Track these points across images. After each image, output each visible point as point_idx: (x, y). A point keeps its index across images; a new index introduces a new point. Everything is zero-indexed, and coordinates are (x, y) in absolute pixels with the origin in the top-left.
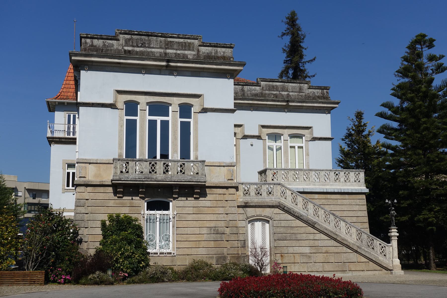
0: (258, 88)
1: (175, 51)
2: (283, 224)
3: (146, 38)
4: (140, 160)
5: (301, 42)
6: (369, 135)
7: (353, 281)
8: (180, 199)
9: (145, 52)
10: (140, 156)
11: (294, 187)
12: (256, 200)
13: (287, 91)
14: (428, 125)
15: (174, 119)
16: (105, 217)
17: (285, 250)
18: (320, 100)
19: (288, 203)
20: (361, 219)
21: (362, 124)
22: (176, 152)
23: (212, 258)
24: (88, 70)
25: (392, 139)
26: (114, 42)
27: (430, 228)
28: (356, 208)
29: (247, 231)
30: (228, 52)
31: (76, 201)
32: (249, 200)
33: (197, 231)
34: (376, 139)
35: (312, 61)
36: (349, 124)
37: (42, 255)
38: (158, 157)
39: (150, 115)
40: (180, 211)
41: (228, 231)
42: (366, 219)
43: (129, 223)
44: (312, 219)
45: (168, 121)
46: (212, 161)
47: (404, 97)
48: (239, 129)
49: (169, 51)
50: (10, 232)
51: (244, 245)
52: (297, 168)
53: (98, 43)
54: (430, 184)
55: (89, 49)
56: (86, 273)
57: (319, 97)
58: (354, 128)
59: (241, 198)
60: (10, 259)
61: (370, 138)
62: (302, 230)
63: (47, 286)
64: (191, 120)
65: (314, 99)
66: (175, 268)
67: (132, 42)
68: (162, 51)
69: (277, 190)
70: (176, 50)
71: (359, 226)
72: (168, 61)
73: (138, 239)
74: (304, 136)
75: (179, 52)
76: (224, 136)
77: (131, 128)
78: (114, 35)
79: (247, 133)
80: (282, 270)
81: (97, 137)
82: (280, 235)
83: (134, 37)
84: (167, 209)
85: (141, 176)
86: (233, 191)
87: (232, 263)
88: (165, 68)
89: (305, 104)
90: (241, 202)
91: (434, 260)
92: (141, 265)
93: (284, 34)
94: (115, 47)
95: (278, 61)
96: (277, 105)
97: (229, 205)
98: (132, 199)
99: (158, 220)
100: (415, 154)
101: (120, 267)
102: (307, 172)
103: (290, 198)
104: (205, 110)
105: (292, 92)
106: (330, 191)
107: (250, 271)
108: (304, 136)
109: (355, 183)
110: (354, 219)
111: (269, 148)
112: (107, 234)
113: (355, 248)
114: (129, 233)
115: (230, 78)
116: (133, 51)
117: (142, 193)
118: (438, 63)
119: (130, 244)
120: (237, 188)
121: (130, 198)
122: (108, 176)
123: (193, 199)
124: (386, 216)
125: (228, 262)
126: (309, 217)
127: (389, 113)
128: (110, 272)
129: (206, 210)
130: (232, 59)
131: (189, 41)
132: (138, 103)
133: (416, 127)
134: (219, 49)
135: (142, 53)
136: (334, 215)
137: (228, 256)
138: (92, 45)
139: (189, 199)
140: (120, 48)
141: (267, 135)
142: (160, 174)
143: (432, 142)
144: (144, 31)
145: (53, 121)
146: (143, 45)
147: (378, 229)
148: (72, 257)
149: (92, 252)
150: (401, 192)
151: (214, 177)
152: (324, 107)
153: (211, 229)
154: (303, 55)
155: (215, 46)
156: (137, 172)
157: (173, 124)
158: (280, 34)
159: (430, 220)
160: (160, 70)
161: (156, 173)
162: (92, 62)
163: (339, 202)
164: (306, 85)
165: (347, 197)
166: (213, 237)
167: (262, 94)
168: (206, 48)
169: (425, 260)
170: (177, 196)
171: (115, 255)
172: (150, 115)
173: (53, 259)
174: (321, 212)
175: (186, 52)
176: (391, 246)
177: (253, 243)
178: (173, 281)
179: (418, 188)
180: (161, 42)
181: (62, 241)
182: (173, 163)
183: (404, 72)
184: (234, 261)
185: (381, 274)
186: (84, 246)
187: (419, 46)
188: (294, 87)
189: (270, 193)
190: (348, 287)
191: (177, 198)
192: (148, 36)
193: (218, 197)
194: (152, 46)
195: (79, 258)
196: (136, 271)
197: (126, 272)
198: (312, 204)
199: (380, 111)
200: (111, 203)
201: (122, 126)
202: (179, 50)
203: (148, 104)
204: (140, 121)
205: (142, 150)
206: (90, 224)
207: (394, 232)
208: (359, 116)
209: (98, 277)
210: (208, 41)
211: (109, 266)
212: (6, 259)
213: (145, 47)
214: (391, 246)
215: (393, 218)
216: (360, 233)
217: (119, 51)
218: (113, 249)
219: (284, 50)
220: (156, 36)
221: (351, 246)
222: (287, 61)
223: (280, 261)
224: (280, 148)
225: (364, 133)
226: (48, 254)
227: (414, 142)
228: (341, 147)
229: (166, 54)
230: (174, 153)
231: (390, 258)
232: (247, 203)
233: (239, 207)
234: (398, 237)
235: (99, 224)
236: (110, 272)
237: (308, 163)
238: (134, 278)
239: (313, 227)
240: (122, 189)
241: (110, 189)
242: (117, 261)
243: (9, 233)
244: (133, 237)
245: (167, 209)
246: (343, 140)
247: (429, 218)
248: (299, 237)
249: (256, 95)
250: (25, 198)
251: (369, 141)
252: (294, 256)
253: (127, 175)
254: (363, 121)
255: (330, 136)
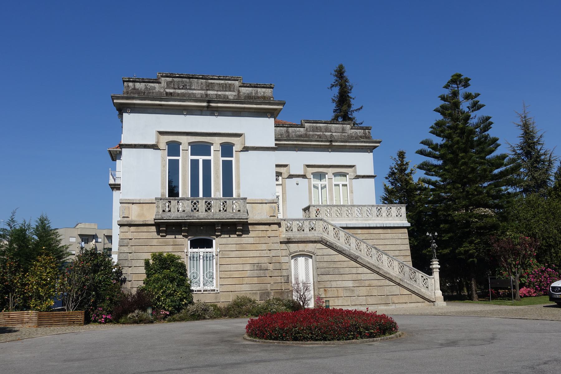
0: (302, 129)
1: (215, 92)
2: (326, 258)
3: (187, 80)
4: (182, 199)
5: (349, 93)
6: (411, 173)
7: (386, 313)
8: (223, 236)
9: (186, 93)
10: (183, 195)
11: (337, 222)
12: (298, 236)
13: (330, 131)
14: (466, 160)
15: (216, 158)
16: (149, 256)
17: (328, 285)
18: (362, 140)
19: (331, 238)
20: (403, 253)
21: (405, 163)
22: (219, 190)
23: (256, 294)
24: (130, 113)
25: (432, 175)
26: (156, 85)
27: (471, 259)
28: (399, 242)
29: (290, 266)
30: (268, 92)
31: (119, 241)
32: (292, 236)
33: (240, 267)
34: (418, 176)
35: (359, 109)
36: (393, 164)
37: (82, 295)
38: (201, 195)
39: (191, 155)
40: (223, 248)
41: (271, 267)
42: (409, 253)
43: (172, 261)
44: (354, 253)
45: (209, 161)
46: (254, 198)
47: (442, 134)
48: (285, 168)
49: (210, 92)
50: (49, 272)
51: (288, 281)
52: (342, 204)
53: (140, 86)
54: (470, 217)
55: (131, 92)
56: (126, 312)
57: (361, 137)
58: (397, 167)
59: (283, 234)
60: (49, 299)
61: (413, 176)
62: (345, 264)
63: (86, 327)
64: (233, 159)
65: (357, 139)
66: (219, 305)
67: (174, 85)
68: (203, 92)
69: (319, 225)
70: (217, 91)
71: (402, 259)
72: (209, 102)
73: (181, 277)
74: (348, 174)
75: (219, 93)
76: (263, 174)
77: (174, 167)
78: (156, 78)
79: (292, 173)
80: (324, 305)
81: (140, 178)
82: (323, 270)
83: (175, 79)
84: (210, 245)
85: (184, 215)
86: (275, 227)
87: (276, 299)
88: (206, 109)
89: (347, 144)
90: (284, 238)
91: (476, 291)
92: (183, 303)
93: (333, 86)
94: (157, 90)
95: (329, 109)
96: (321, 145)
97: (272, 241)
98: (175, 238)
99: (201, 257)
100: (454, 188)
101: (161, 305)
102: (349, 208)
103: (332, 232)
104: (246, 149)
105: (335, 132)
106: (372, 226)
107: (293, 307)
108: (348, 174)
109: (397, 218)
110: (397, 253)
111: (314, 186)
112: (150, 272)
113: (398, 281)
114: (172, 272)
115: (270, 117)
116: (175, 93)
117: (185, 231)
118: (474, 101)
119: (172, 282)
120: (279, 224)
121: (173, 236)
122: (150, 216)
123: (236, 236)
124: (429, 249)
125: (271, 297)
126: (352, 251)
127: (429, 150)
128: (150, 311)
129: (248, 247)
130: (272, 99)
131: (230, 82)
132: (180, 144)
133: (454, 162)
134: (259, 90)
135: (183, 95)
136: (376, 248)
137: (272, 291)
138: (134, 89)
139: (231, 236)
140: (162, 90)
141: (312, 174)
142: (202, 212)
143: (470, 176)
144: (185, 73)
145: (114, 169)
146: (184, 87)
147: (421, 263)
148: (113, 296)
149: (134, 291)
150: (442, 226)
151: (256, 214)
152: (366, 146)
153: (254, 266)
154: (351, 105)
155: (255, 87)
156: (180, 210)
157: (215, 163)
158: (330, 86)
159: (471, 252)
160: (201, 110)
161: (198, 211)
162: (134, 104)
163: (382, 236)
164: (349, 126)
165: (389, 231)
166: (256, 273)
167: (306, 135)
168: (247, 88)
169: (468, 291)
170: (219, 233)
171: (156, 293)
172: (191, 155)
173: (94, 299)
174: (363, 246)
175: (227, 93)
176: (433, 278)
177: (297, 279)
178: (215, 318)
179: (459, 221)
180: (202, 84)
181: (104, 281)
182: (215, 201)
183: (442, 110)
184: (278, 296)
185: (424, 306)
186: (128, 285)
187: (456, 86)
188: (337, 128)
189: (312, 229)
190: (380, 321)
191: (220, 235)
192: (189, 78)
193: (261, 234)
194: (193, 88)
195: (121, 297)
196: (178, 309)
197: (168, 310)
198: (354, 239)
199: (420, 149)
200: (155, 242)
201: (164, 166)
202: (220, 91)
203: (190, 144)
204: (182, 161)
205: (185, 189)
206: (134, 263)
207: (436, 265)
208: (401, 155)
209: (137, 316)
210: (248, 82)
211: (149, 305)
212: (46, 300)
213: (186, 89)
214: (433, 278)
215: (435, 251)
216: (402, 266)
217: (161, 93)
218: (155, 288)
219: (334, 100)
220: (197, 78)
221: (393, 279)
222: (336, 110)
223: (323, 296)
224: (325, 187)
225: (406, 172)
226: (89, 294)
227: (453, 176)
228: (385, 185)
229: (207, 95)
230: (217, 190)
231: (432, 290)
232: (290, 239)
233: (281, 243)
234: (439, 269)
235: (142, 263)
236: (150, 311)
237: (352, 200)
238: (175, 316)
239: (356, 261)
240: (166, 228)
241: (154, 229)
242: (158, 299)
243: (48, 273)
244: (175, 275)
245: (210, 245)
246: (386, 178)
247: (470, 250)
248: (342, 271)
249: (301, 136)
250: (104, 244)
251: (411, 179)
252: (338, 290)
253: (169, 214)
254: (406, 160)
255: (373, 174)
